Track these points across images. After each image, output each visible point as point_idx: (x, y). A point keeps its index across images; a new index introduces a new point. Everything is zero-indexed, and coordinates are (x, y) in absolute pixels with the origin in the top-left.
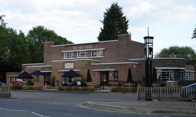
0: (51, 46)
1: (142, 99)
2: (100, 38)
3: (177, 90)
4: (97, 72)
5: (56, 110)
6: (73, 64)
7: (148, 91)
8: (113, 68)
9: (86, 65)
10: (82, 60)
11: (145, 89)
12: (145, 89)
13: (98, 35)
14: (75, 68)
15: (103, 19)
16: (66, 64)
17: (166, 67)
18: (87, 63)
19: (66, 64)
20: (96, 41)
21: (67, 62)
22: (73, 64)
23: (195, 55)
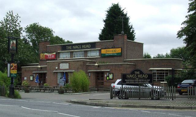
0: (47, 46)
1: (114, 97)
2: (101, 37)
3: (170, 89)
4: (92, 73)
5: (39, 106)
6: (68, 64)
7: (192, 90)
8: (108, 69)
9: (81, 65)
10: (77, 61)
11: (193, 89)
12: (193, 89)
13: (100, 32)
14: (70, 68)
15: (104, 17)
16: (61, 65)
17: (161, 68)
18: (82, 63)
19: (61, 65)
20: (96, 39)
21: (62, 62)
22: (68, 64)
23: (1, 70)
